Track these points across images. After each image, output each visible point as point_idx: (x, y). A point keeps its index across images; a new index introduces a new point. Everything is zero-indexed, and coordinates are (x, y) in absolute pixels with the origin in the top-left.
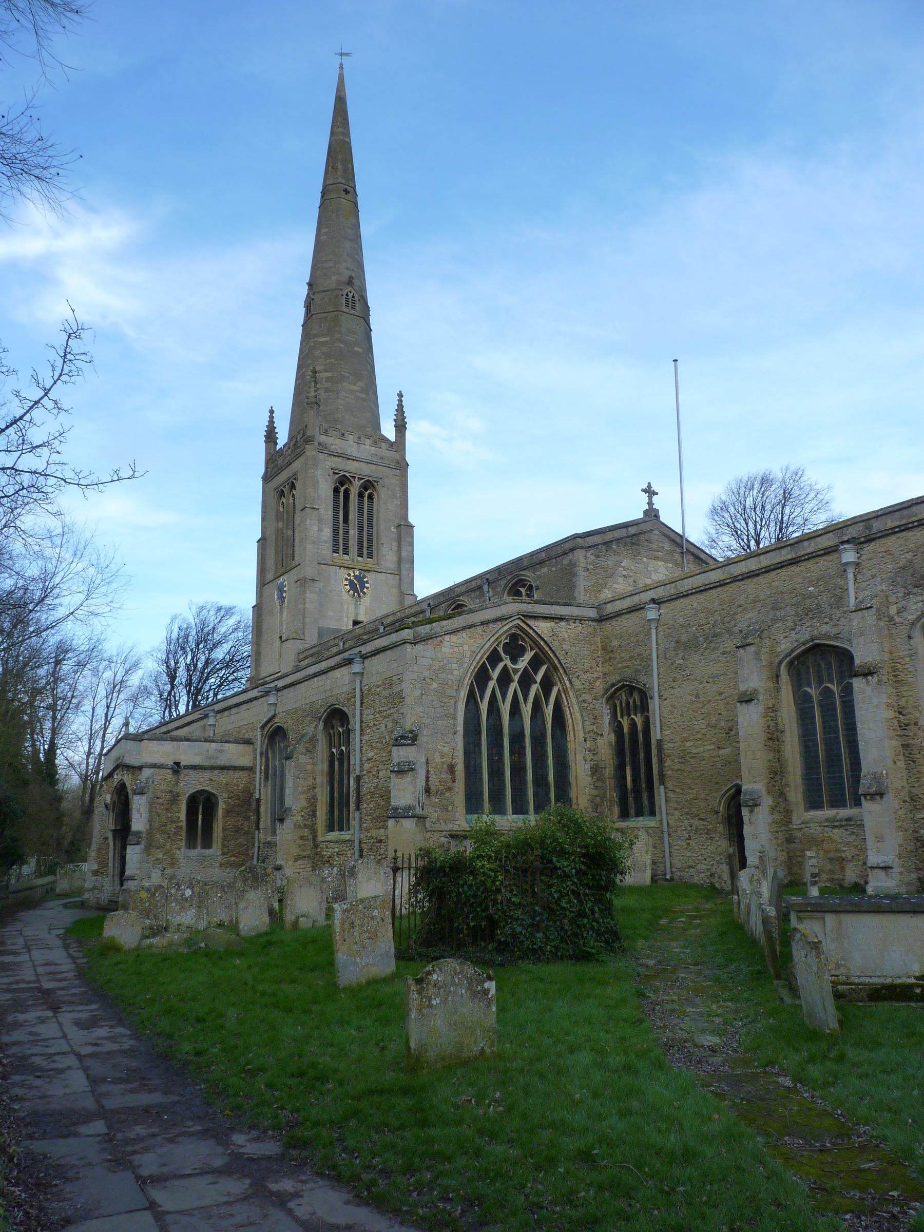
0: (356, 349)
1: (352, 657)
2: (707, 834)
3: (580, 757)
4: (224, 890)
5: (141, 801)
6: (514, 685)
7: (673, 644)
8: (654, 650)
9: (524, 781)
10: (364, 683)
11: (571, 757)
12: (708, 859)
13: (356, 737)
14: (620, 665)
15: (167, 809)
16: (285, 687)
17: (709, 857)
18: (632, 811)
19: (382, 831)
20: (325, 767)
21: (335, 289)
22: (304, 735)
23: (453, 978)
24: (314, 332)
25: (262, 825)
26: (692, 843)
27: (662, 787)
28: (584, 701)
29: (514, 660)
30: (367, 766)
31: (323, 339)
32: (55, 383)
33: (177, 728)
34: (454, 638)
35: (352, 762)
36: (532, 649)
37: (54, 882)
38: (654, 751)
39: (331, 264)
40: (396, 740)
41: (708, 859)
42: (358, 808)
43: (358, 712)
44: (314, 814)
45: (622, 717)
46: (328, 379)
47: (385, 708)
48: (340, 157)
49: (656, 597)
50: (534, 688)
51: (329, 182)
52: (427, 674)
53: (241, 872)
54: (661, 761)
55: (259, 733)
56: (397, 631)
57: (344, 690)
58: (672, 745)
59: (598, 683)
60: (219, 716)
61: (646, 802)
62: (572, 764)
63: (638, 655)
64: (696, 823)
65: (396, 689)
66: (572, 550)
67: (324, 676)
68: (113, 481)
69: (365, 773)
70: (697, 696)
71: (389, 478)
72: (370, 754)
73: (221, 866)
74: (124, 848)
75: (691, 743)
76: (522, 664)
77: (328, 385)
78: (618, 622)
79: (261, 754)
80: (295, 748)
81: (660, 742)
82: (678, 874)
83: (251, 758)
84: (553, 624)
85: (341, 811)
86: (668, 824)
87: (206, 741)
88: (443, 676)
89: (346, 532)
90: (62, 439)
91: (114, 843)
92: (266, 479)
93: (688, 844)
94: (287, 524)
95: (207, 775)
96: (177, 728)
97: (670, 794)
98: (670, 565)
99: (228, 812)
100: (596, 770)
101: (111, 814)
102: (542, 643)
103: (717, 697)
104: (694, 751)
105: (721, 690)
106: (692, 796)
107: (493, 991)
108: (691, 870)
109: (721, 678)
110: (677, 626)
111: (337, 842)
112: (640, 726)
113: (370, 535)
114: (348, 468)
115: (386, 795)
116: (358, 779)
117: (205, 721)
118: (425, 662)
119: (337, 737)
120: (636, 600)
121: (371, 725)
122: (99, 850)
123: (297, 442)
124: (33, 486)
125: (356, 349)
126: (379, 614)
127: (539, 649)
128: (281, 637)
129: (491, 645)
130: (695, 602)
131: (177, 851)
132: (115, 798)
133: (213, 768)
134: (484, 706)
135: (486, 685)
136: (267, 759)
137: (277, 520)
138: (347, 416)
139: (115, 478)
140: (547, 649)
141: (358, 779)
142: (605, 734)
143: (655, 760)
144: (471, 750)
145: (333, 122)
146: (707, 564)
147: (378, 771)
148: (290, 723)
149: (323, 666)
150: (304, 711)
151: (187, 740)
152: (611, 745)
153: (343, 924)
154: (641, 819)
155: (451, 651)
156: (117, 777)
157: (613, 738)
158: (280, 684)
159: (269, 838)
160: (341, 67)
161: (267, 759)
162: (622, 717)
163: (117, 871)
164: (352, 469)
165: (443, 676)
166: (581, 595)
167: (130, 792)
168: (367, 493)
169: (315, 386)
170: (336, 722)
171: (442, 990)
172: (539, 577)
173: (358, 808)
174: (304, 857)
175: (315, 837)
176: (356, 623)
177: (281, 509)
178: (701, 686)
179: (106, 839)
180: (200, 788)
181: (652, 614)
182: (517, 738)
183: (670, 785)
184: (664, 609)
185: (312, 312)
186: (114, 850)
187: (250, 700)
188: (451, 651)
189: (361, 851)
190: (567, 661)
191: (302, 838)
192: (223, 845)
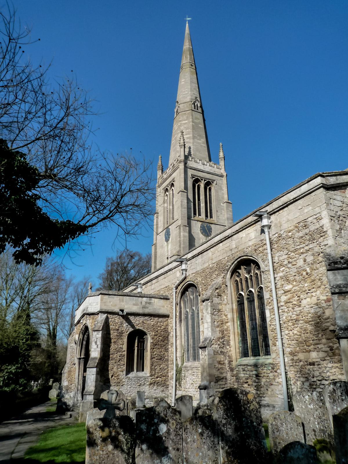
0: (200, 126)
5: (97, 336)
16: (193, 257)
31: (184, 122)
39: (187, 92)
56: (308, 182)
57: (250, 243)
60: (144, 287)
73: (151, 384)
74: (85, 371)
89: (199, 205)
94: (170, 203)
99: (154, 345)
101: (78, 347)
114: (199, 175)
119: (244, 282)
121: (286, 262)
122: (70, 371)
123: (174, 165)
125: (200, 126)
133: (144, 315)
136: (180, 308)
147: (300, 300)
150: (211, 269)
156: (83, 321)
161: (180, 308)
163: (80, 387)
164: (201, 176)
168: (208, 188)
170: (243, 271)
177: (166, 198)
186: (79, 372)
187: (166, 272)
192: (151, 369)
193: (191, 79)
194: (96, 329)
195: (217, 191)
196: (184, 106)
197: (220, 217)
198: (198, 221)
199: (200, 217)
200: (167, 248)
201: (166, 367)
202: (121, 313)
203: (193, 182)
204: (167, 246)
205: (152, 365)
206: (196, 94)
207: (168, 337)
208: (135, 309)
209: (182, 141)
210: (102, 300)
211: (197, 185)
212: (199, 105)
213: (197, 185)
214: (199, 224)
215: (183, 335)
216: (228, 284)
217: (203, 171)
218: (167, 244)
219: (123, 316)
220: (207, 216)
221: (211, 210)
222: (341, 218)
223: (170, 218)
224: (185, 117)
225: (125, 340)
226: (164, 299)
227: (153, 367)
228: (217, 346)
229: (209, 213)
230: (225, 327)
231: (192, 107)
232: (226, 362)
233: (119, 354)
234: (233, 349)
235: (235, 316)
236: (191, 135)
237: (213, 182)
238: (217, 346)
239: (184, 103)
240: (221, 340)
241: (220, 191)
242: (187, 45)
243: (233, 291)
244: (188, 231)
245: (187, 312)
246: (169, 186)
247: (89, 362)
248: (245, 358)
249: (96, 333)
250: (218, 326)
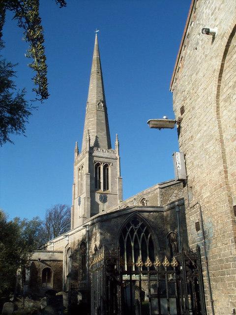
107: (60, 313)
193: (97, 84)
195: (112, 171)
208: (46, 258)
209: (88, 137)
214: (99, 194)
224: (92, 116)
229: (106, 187)
236: (96, 130)
241: (114, 172)
242: (95, 55)
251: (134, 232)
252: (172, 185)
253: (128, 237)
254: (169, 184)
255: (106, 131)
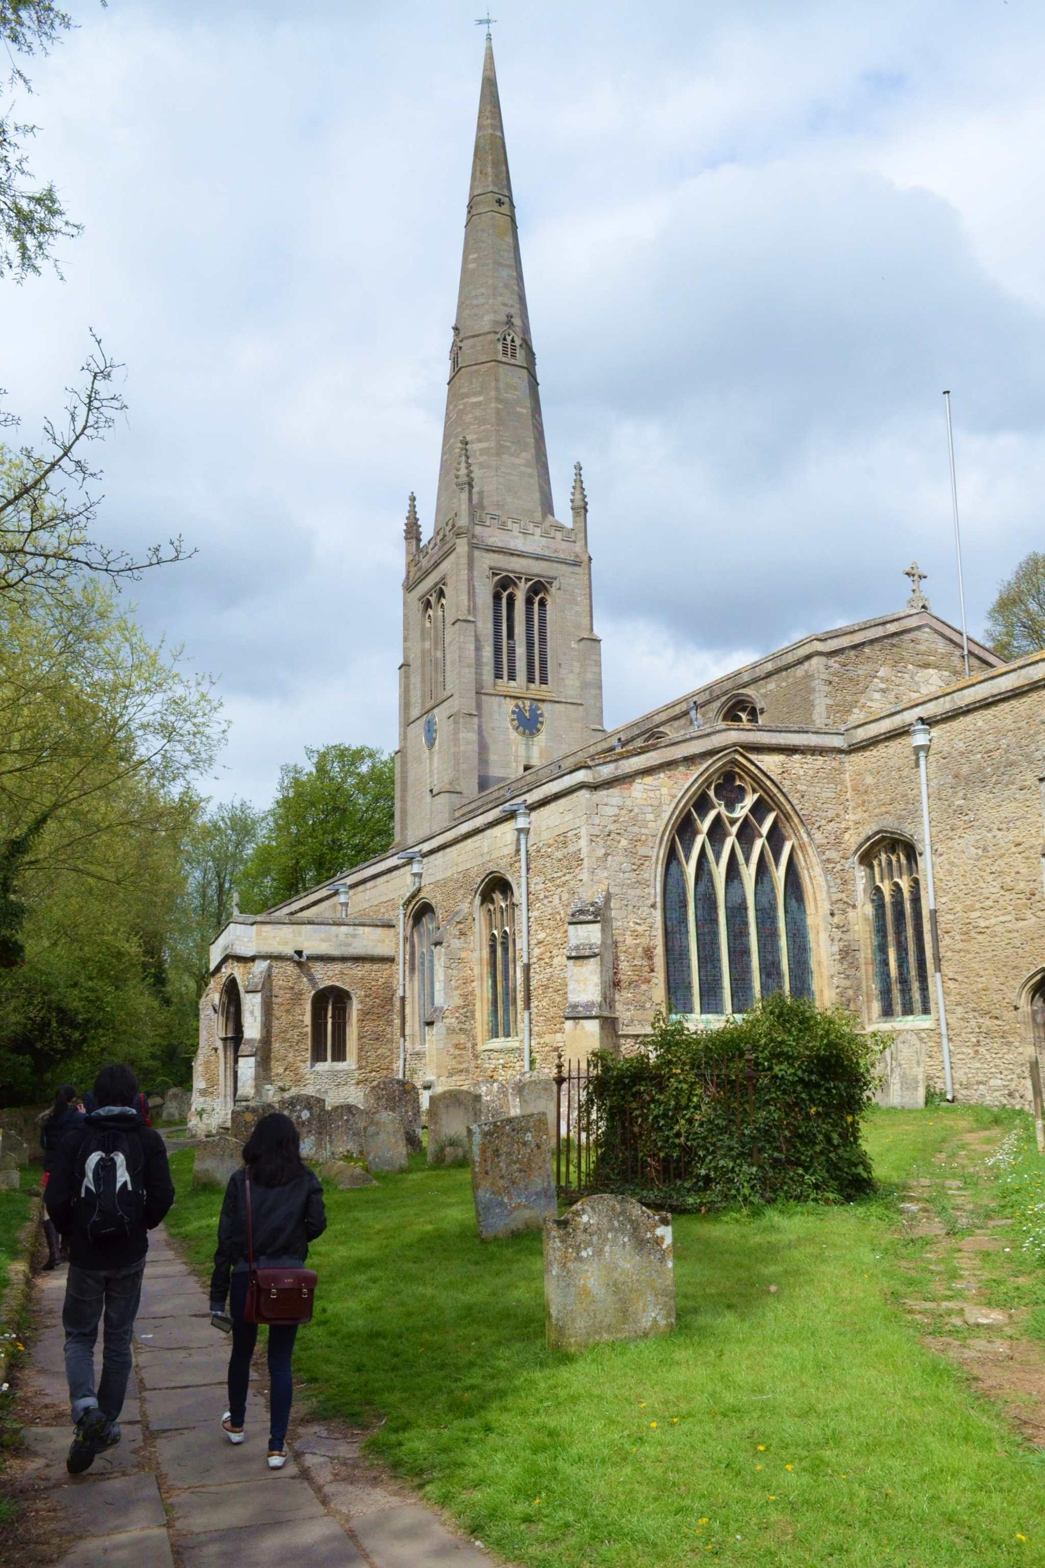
0: (518, 409)
1: (515, 808)
2: (1003, 1037)
3: (823, 937)
4: (351, 1112)
5: (254, 1000)
6: (730, 841)
7: (950, 779)
8: (924, 788)
9: (747, 970)
10: (531, 842)
11: (811, 936)
12: (1005, 1072)
13: (522, 914)
14: (877, 811)
15: (288, 1011)
16: (432, 852)
17: (1006, 1069)
18: (898, 1008)
19: (559, 1036)
20: (486, 953)
21: (489, 333)
22: (457, 913)
23: (610, 1221)
24: (465, 390)
25: (407, 1032)
26: (981, 1049)
27: (938, 975)
28: (828, 860)
29: (730, 806)
30: (536, 952)
31: (474, 400)
32: (77, 438)
33: (302, 909)
34: (648, 780)
35: (518, 947)
36: (754, 791)
37: (161, 1106)
38: (927, 926)
39: (482, 300)
40: (573, 915)
41: (1005, 1072)
42: (528, 1006)
43: (523, 881)
44: (470, 1016)
45: (882, 881)
46: (483, 452)
47: (559, 874)
48: (491, 154)
49: (925, 715)
50: (759, 844)
51: (476, 193)
52: (612, 827)
53: (373, 1088)
54: (936, 940)
55: (402, 912)
58: (952, 917)
59: (847, 836)
60: (351, 892)
61: (916, 995)
62: (812, 945)
63: (903, 796)
64: (987, 1022)
65: (571, 849)
66: (808, 657)
67: (480, 836)
68: (151, 564)
69: (534, 960)
70: (985, 849)
71: (566, 579)
72: (541, 936)
73: (358, 1084)
74: (236, 1062)
75: (977, 914)
76: (742, 811)
77: (482, 459)
78: (874, 752)
79: (405, 939)
80: (445, 928)
81: (934, 913)
82: (964, 1092)
83: (393, 944)
84: (782, 758)
85: (506, 1011)
86: (947, 1024)
87: (335, 924)
88: (636, 829)
89: (512, 651)
90: (90, 516)
91: (225, 1054)
92: (409, 586)
93: (977, 1052)
95: (338, 967)
96: (302, 909)
97: (951, 984)
98: (947, 673)
99: (364, 1014)
100: (846, 953)
101: (221, 1017)
102: (768, 783)
103: (1014, 849)
104: (983, 925)
105: (1019, 840)
106: (980, 986)
107: (668, 1241)
108: (981, 1087)
109: (1018, 823)
110: (955, 754)
111: (501, 1051)
112: (906, 895)
113: (543, 653)
114: (510, 567)
115: (562, 990)
116: (527, 968)
117: (335, 899)
118: (610, 811)
119: (498, 915)
120: (896, 721)
121: (542, 896)
122: (207, 1063)
123: (445, 536)
124: (40, 571)
125: (518, 409)
126: (556, 755)
127: (764, 791)
128: (431, 791)
129: (699, 788)
130: (978, 719)
131: (302, 1064)
132: (225, 999)
133: (343, 959)
134: (691, 869)
135: (692, 841)
136: (413, 946)
137: (423, 639)
138: (509, 499)
139: (154, 561)
140: (775, 790)
141: (527, 968)
142: (859, 904)
143: (927, 937)
144: (674, 931)
145: (480, 112)
146: (991, 666)
148: (439, 897)
149: (479, 821)
151: (309, 923)
152: (866, 919)
153: (483, 1151)
154: (910, 1018)
155: (645, 796)
156: (226, 971)
157: (869, 910)
158: (426, 847)
159: (418, 1048)
160: (489, 38)
161: (413, 946)
162: (882, 881)
163: (230, 1091)
165: (636, 829)
166: (819, 717)
167: (241, 989)
168: (537, 599)
169: (467, 462)
170: (497, 896)
171: (595, 1238)
172: (765, 696)
173: (528, 1006)
174: (462, 1071)
175: (474, 1045)
176: (527, 768)
177: (428, 625)
178: (989, 835)
179: (216, 1049)
180: (331, 983)
181: (920, 739)
182: (737, 912)
183: (948, 969)
184: (935, 732)
185: (460, 365)
186: (226, 1063)
187: (390, 870)
188: (645, 796)
189: (532, 1062)
190: (804, 808)
191: (457, 1046)
192: (360, 1058)
194: (250, 988)
196: (473, 346)
197: (566, 681)
198: (506, 696)
199: (512, 683)
200: (431, 764)
201: (389, 1053)
202: (296, 957)
203: (496, 585)
204: (431, 759)
205: (361, 1049)
206: (510, 302)
207: (391, 999)
209: (463, 471)
210: (258, 934)
211: (505, 594)
212: (518, 342)
213: (505, 594)
214: (510, 705)
215: (416, 995)
216: (476, 916)
217: (521, 555)
218: (431, 754)
219: (299, 964)
220: (531, 680)
221: (543, 662)
222: (613, 835)
223: (436, 682)
225: (308, 1007)
226: (383, 926)
227: (363, 1053)
228: (453, 1020)
230: (471, 989)
231: (496, 352)
232: (469, 1045)
233: (296, 1031)
234: (478, 1025)
235: (485, 971)
236: (493, 444)
237: (551, 583)
238: (453, 1020)
239: (473, 336)
240: (461, 1011)
243: (484, 927)
244: (476, 727)
245: (423, 953)
246: (434, 595)
247: (242, 1047)
248: (495, 1040)
249: (251, 995)
250: (457, 988)
251: (725, 834)
252: (872, 642)
253: (703, 853)
254: (858, 638)
255: (533, 451)
